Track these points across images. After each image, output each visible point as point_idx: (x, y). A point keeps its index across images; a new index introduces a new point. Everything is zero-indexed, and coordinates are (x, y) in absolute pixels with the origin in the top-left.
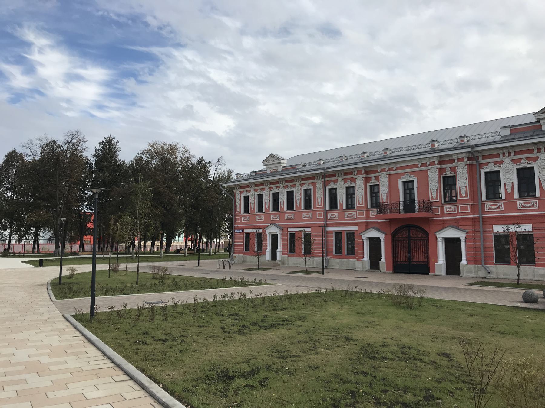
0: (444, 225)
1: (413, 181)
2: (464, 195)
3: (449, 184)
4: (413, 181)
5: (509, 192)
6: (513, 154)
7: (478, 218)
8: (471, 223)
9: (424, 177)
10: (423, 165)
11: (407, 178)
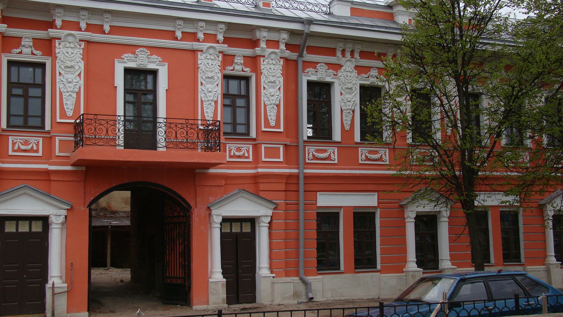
0: (231, 185)
1: (154, 73)
2: (273, 123)
3: (238, 92)
4: (154, 73)
5: (347, 128)
6: (357, 55)
7: (297, 176)
8: (282, 187)
9: (185, 66)
10: (193, 37)
11: (143, 60)
